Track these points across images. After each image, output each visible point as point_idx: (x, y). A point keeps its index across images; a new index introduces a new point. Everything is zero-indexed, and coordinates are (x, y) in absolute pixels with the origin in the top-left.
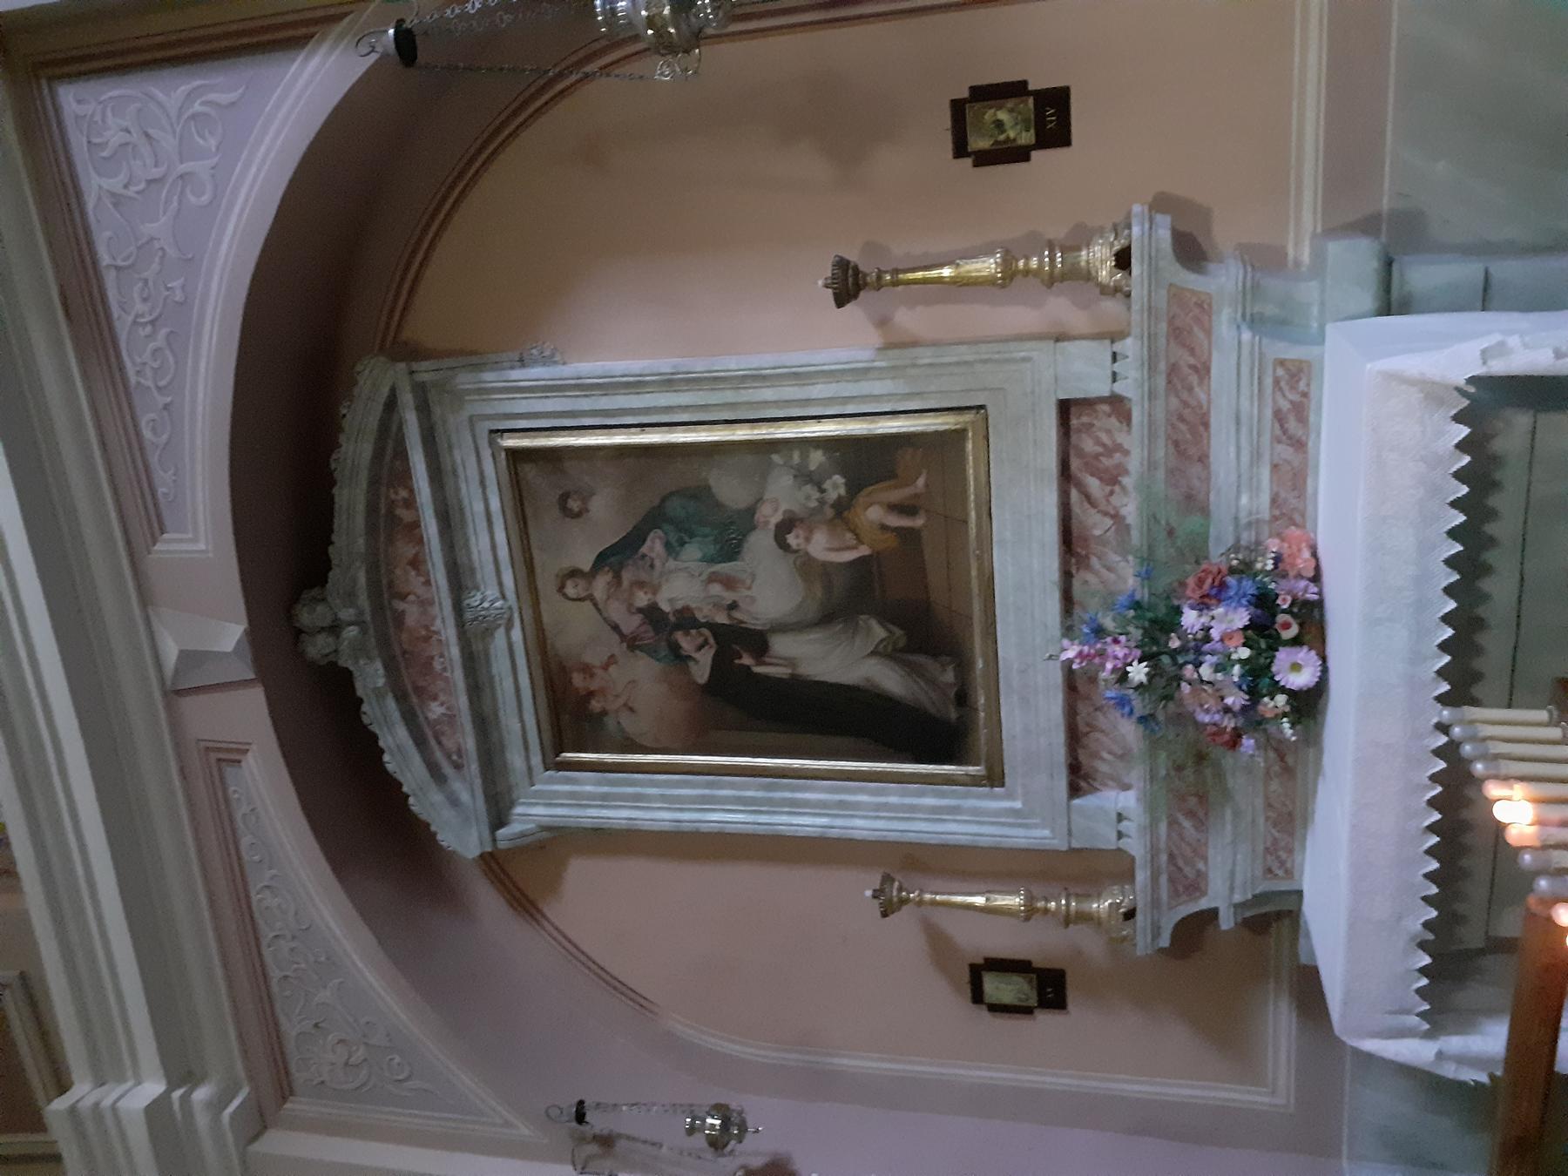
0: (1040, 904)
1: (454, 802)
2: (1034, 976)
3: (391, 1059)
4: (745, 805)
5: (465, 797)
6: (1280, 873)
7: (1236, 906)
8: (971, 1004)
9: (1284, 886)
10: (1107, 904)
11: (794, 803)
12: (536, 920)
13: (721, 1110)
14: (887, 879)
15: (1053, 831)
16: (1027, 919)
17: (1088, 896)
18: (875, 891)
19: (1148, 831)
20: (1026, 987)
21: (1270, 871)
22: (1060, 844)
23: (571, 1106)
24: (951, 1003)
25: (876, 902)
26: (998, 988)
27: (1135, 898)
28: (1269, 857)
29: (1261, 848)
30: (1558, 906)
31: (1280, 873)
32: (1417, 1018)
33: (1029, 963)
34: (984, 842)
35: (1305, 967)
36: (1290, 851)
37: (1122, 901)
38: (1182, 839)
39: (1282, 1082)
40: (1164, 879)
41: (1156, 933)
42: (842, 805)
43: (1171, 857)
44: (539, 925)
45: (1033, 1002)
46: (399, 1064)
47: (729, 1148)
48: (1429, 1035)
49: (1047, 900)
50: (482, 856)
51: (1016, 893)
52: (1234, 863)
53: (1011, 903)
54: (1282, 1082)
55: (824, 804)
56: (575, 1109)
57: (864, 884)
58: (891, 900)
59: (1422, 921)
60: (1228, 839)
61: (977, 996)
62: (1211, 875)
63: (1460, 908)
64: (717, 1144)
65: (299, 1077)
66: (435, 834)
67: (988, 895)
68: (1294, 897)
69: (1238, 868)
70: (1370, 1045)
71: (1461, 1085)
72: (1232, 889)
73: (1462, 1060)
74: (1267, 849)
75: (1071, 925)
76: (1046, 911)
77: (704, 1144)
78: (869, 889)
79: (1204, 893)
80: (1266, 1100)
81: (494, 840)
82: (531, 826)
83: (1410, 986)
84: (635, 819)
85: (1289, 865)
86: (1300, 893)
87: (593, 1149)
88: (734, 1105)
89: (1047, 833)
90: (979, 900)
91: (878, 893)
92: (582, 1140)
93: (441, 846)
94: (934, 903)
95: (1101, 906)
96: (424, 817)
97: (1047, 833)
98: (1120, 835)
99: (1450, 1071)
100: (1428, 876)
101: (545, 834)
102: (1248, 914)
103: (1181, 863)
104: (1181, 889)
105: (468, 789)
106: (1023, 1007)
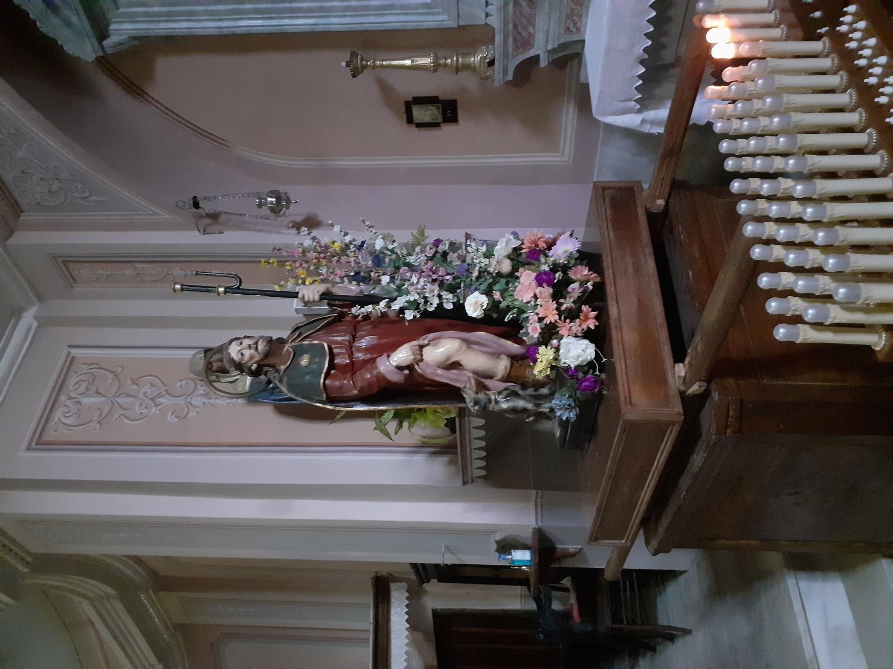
0: (442, 61)
1: (69, 25)
2: (440, 105)
3: (77, 186)
4: (260, 14)
5: (74, 19)
6: (574, 30)
7: (549, 52)
8: (406, 125)
9: (575, 38)
10: (479, 58)
11: (292, 10)
12: (146, 100)
13: (273, 193)
14: (354, 55)
15: (449, 16)
16: (435, 71)
17: (469, 54)
18: (347, 62)
19: (502, 9)
20: (436, 112)
21: (568, 29)
22: (452, 24)
23: (189, 200)
24: (395, 125)
25: (349, 69)
26: (421, 114)
27: (494, 53)
28: (568, 21)
29: (564, 17)
30: (706, 16)
31: (574, 30)
32: (635, 103)
33: (437, 97)
34: (409, 26)
35: (584, 84)
36: (580, 16)
37: (487, 55)
38: (521, 14)
39: (567, 150)
40: (510, 39)
41: (505, 73)
42: (322, 9)
43: (515, 26)
44: (143, 98)
45: (440, 120)
46: (82, 188)
47: (282, 212)
48: (639, 111)
49: (446, 59)
50: (97, 58)
51: (428, 56)
52: (549, 26)
53: (426, 62)
54: (567, 150)
55: (311, 10)
56: (192, 201)
57: (341, 59)
58: (357, 67)
59: (643, 48)
60: (546, 11)
61: (410, 120)
62: (537, 35)
63: (664, 40)
64: (275, 210)
65: (23, 202)
66: (62, 46)
67: (412, 59)
68: (581, 44)
69: (551, 29)
70: (610, 120)
71: (651, 135)
72: (547, 43)
73: (653, 123)
74: (567, 16)
75: (459, 72)
76: (446, 65)
77: (269, 212)
78: (343, 61)
79: (532, 47)
80: (558, 159)
81: (103, 48)
82: (124, 37)
83: (633, 86)
84: (192, 28)
85: (579, 25)
86: (583, 42)
87: (207, 221)
88: (281, 190)
89: (445, 17)
90: (408, 62)
91: (349, 64)
92: (200, 217)
93: (68, 54)
94: (382, 66)
95: (475, 59)
96: (51, 35)
97: (445, 17)
98: (487, 15)
99: (647, 129)
100: (649, 21)
101: (135, 42)
102: (555, 57)
103: (520, 29)
104: (520, 45)
105: (79, 19)
106: (434, 123)
